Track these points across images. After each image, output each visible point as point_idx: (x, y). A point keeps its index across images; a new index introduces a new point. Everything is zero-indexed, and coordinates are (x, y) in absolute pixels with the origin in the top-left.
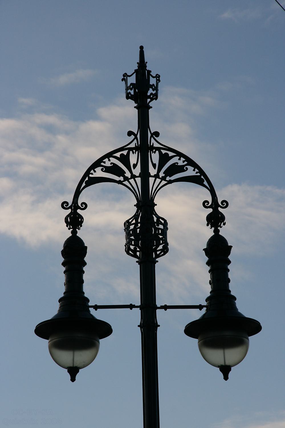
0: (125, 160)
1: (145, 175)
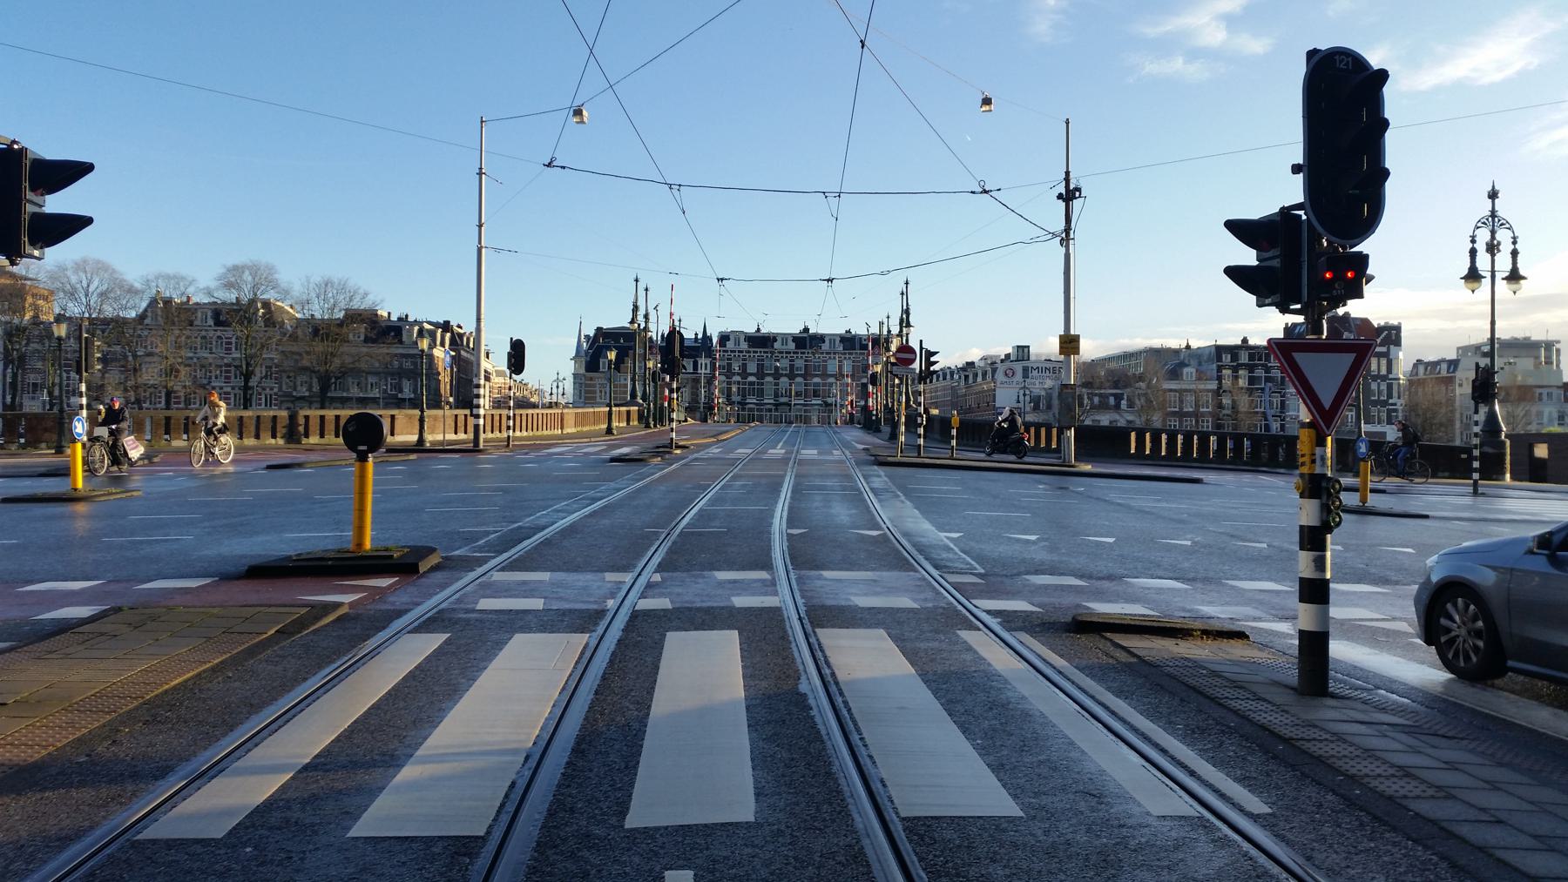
0: (1487, 219)
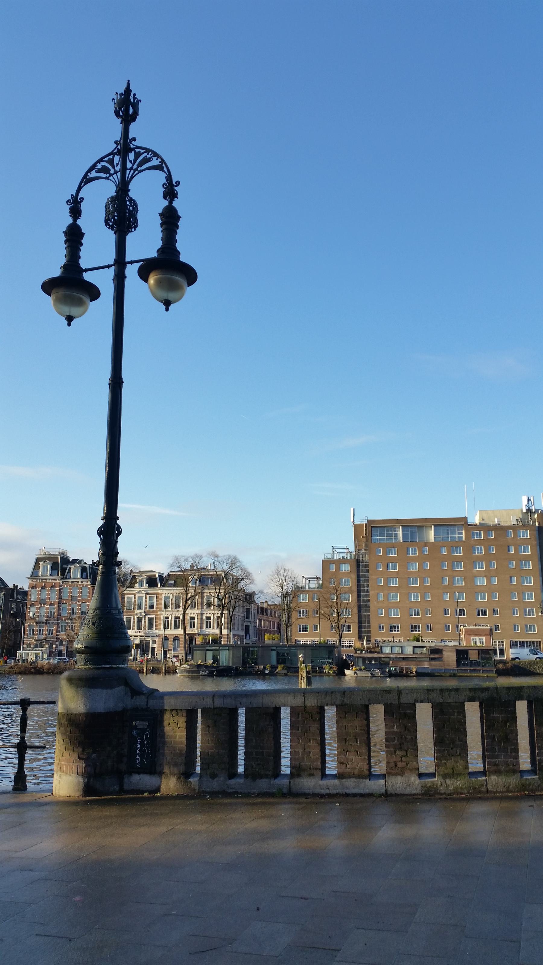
0: (111, 162)
1: (124, 169)
